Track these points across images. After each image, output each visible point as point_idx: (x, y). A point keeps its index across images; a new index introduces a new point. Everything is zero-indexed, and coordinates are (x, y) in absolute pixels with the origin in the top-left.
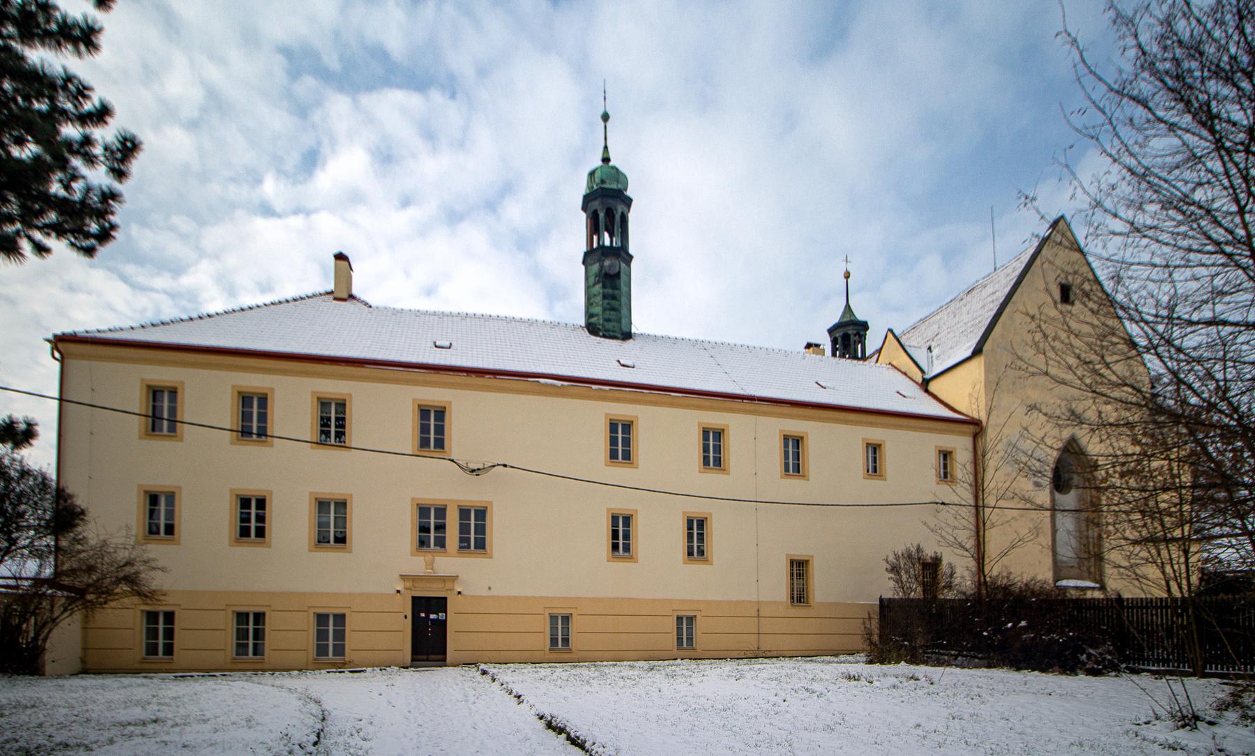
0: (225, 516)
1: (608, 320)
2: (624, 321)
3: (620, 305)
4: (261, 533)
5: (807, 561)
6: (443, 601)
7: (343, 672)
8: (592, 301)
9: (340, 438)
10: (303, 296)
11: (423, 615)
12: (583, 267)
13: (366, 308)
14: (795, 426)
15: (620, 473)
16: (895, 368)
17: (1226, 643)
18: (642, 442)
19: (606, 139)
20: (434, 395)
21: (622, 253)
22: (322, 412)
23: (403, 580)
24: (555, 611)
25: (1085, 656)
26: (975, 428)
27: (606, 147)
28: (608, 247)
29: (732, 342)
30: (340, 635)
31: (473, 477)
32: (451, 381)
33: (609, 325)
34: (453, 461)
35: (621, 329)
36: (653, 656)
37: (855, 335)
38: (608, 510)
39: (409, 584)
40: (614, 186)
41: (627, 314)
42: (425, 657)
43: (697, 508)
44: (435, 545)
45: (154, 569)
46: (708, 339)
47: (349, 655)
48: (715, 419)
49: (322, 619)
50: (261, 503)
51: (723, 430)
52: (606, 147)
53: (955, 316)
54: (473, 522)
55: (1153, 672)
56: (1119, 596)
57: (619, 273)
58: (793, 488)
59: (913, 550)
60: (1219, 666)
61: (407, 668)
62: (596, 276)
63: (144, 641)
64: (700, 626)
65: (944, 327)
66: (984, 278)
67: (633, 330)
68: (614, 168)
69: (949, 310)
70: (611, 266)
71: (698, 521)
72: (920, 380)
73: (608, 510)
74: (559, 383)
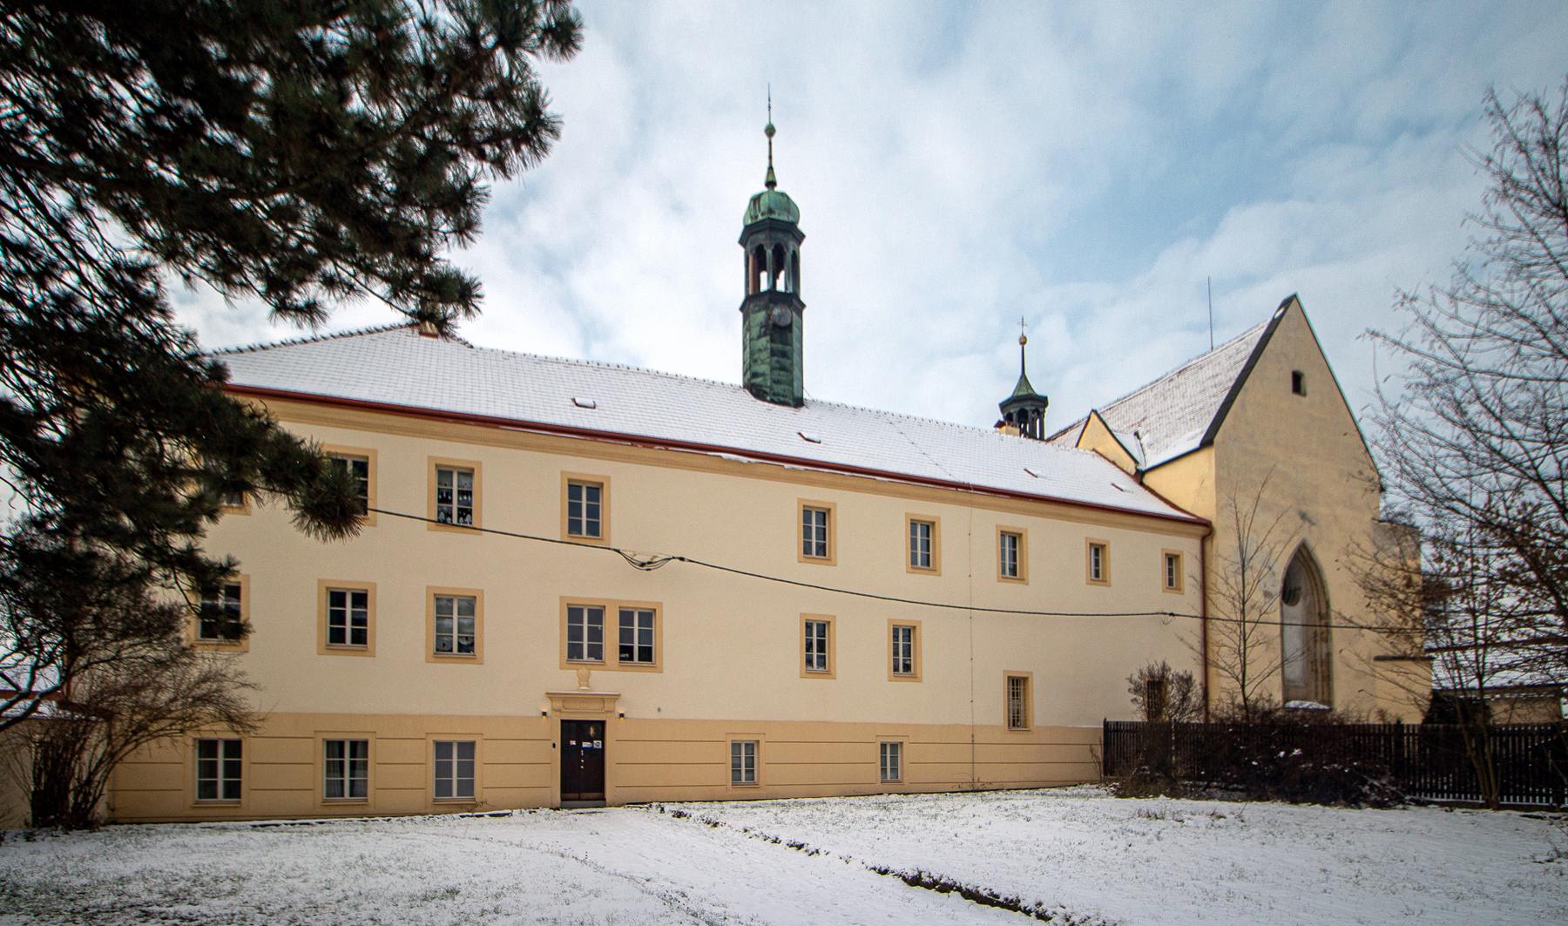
0: (312, 616)
1: (777, 382)
3: (792, 365)
4: (360, 637)
5: (1025, 679)
6: (601, 726)
7: (482, 816)
8: (756, 356)
9: (464, 517)
10: (380, 327)
12: (740, 315)
13: (465, 348)
14: (1014, 520)
15: (815, 571)
16: (1101, 455)
17: (1561, 775)
18: (842, 533)
19: (770, 157)
20: (587, 467)
21: (794, 301)
22: (439, 484)
23: (551, 699)
24: (738, 738)
25: (1367, 787)
26: (1204, 529)
27: (771, 168)
28: (780, 293)
29: (919, 415)
30: (467, 769)
31: (643, 572)
32: (366, 420)
33: (779, 388)
34: (618, 551)
35: (793, 393)
37: (1033, 412)
38: (802, 615)
39: (558, 705)
40: (784, 217)
41: (799, 375)
42: (576, 795)
43: (905, 615)
44: (589, 655)
45: (244, 685)
46: (891, 410)
48: (925, 509)
49: (443, 748)
50: (360, 599)
51: (829, 510)
52: (771, 168)
53: (1165, 399)
54: (636, 628)
55: (1442, 805)
56: (1399, 722)
58: (1010, 594)
60: (1518, 797)
61: (558, 809)
62: (762, 327)
63: (197, 778)
65: (1153, 411)
66: (1198, 358)
67: (805, 396)
68: (783, 195)
69: (1155, 391)
70: (780, 316)
71: (818, 625)
72: (1133, 472)
73: (802, 615)
74: (745, 459)
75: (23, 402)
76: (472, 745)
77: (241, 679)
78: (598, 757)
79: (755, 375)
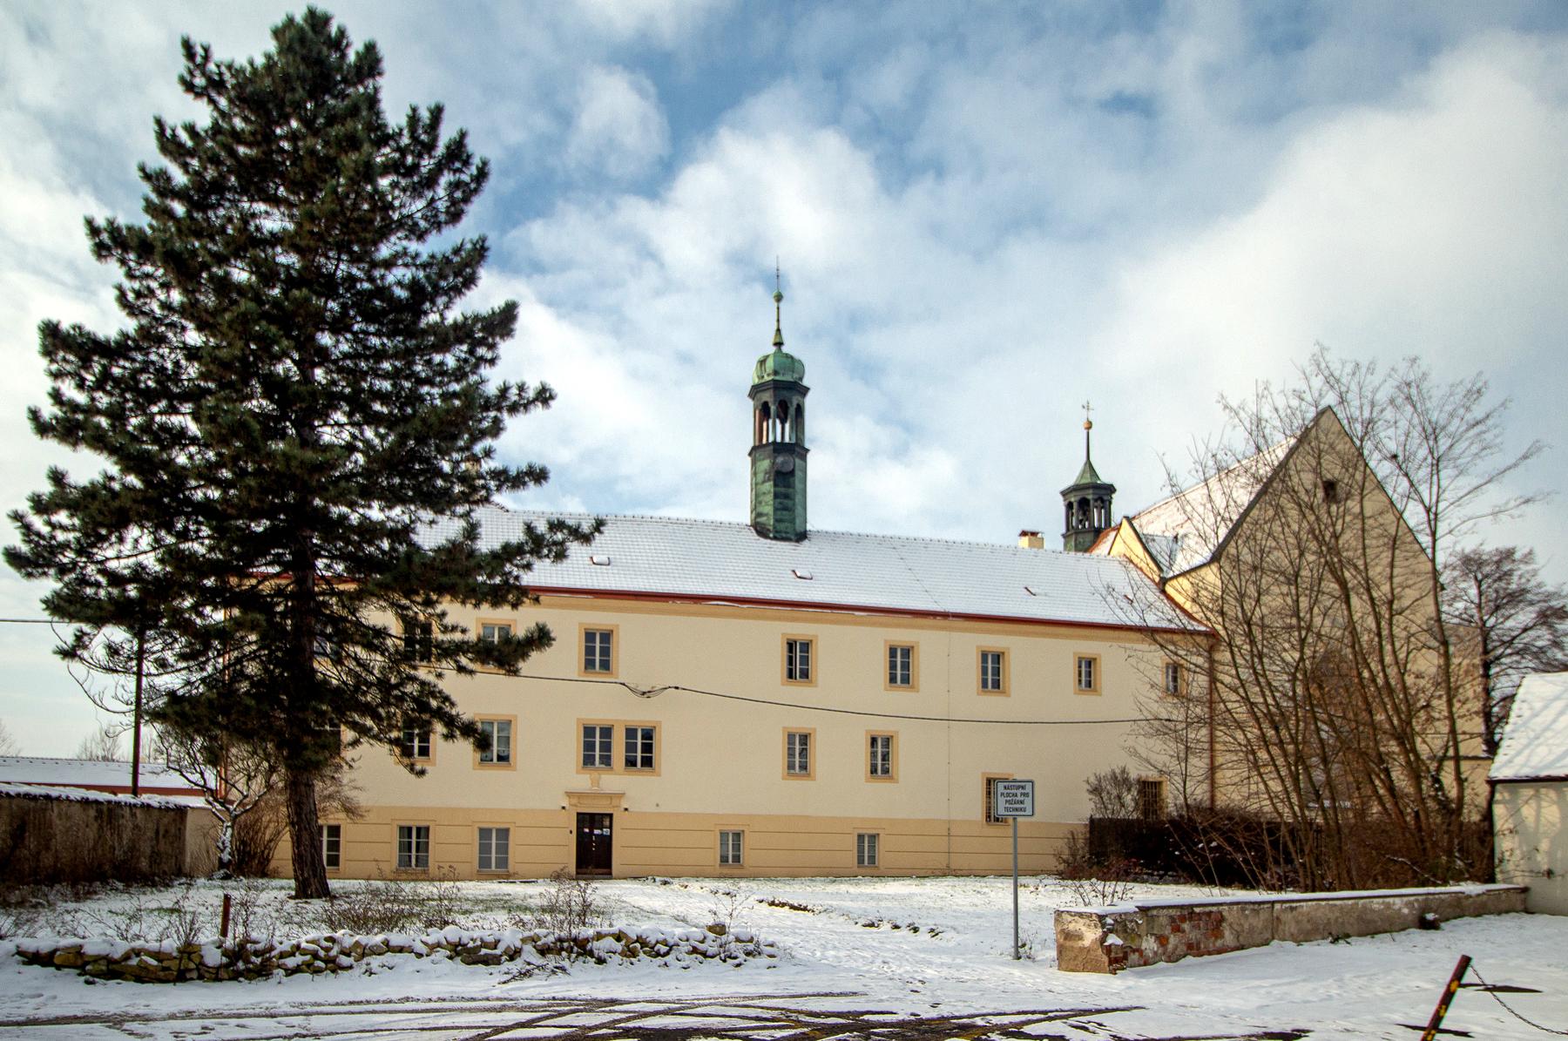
2: (798, 521)
11: (587, 830)
14: (994, 640)
21: (797, 449)
24: (726, 828)
27: (778, 330)
30: (503, 849)
31: (644, 699)
33: (781, 526)
36: (835, 874)
37: (1096, 500)
39: (574, 801)
43: (881, 727)
45: (356, 788)
47: (512, 866)
49: (485, 833)
52: (778, 330)
57: (793, 471)
58: (992, 704)
59: (1118, 771)
64: (883, 846)
67: (809, 527)
68: (787, 356)
70: (783, 463)
75: (208, 610)
76: (507, 831)
77: (353, 784)
78: (607, 842)
79: (759, 515)
